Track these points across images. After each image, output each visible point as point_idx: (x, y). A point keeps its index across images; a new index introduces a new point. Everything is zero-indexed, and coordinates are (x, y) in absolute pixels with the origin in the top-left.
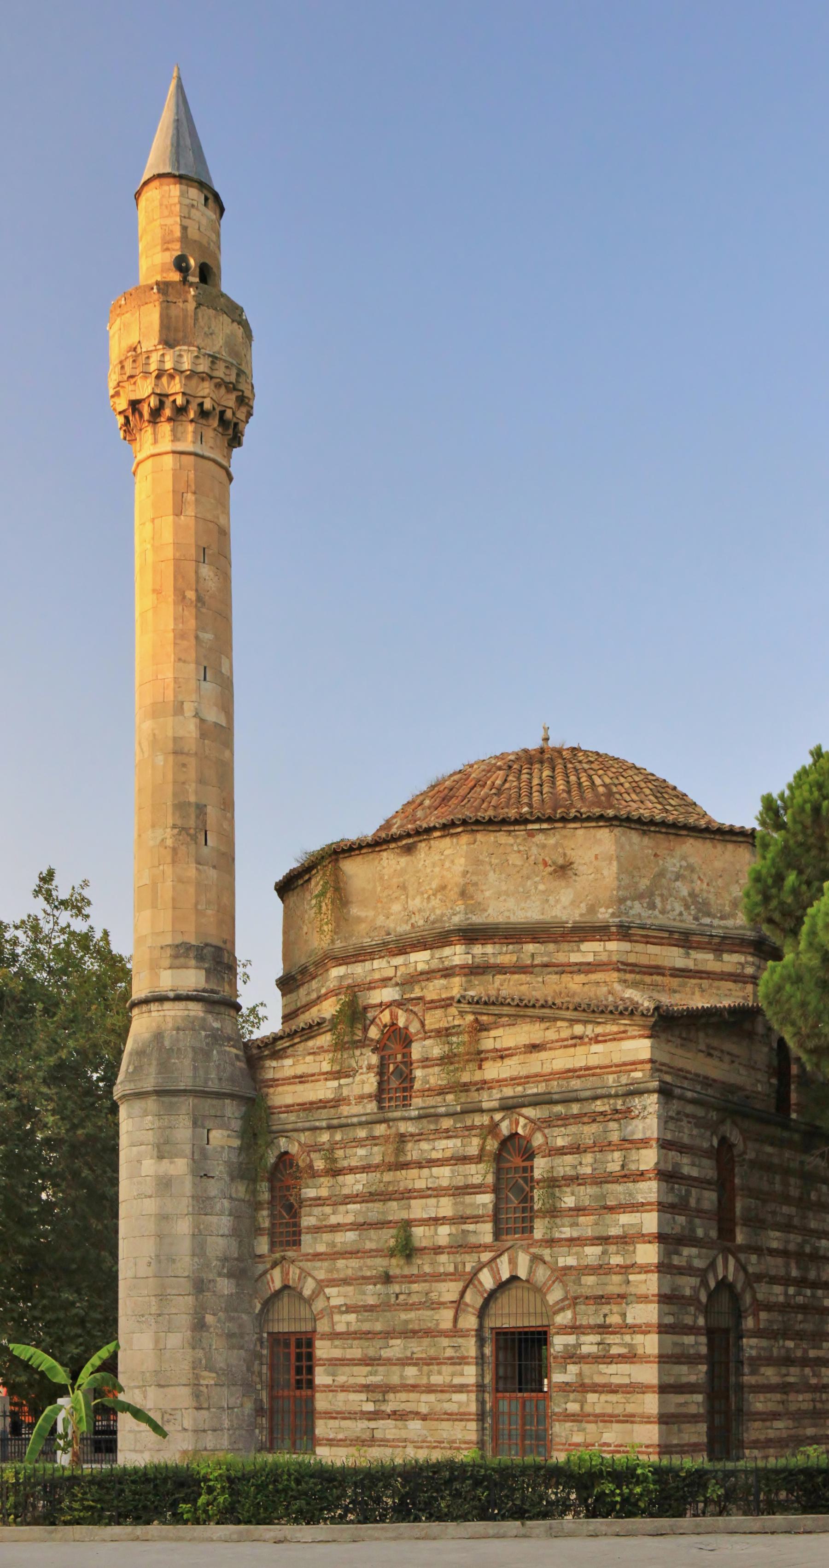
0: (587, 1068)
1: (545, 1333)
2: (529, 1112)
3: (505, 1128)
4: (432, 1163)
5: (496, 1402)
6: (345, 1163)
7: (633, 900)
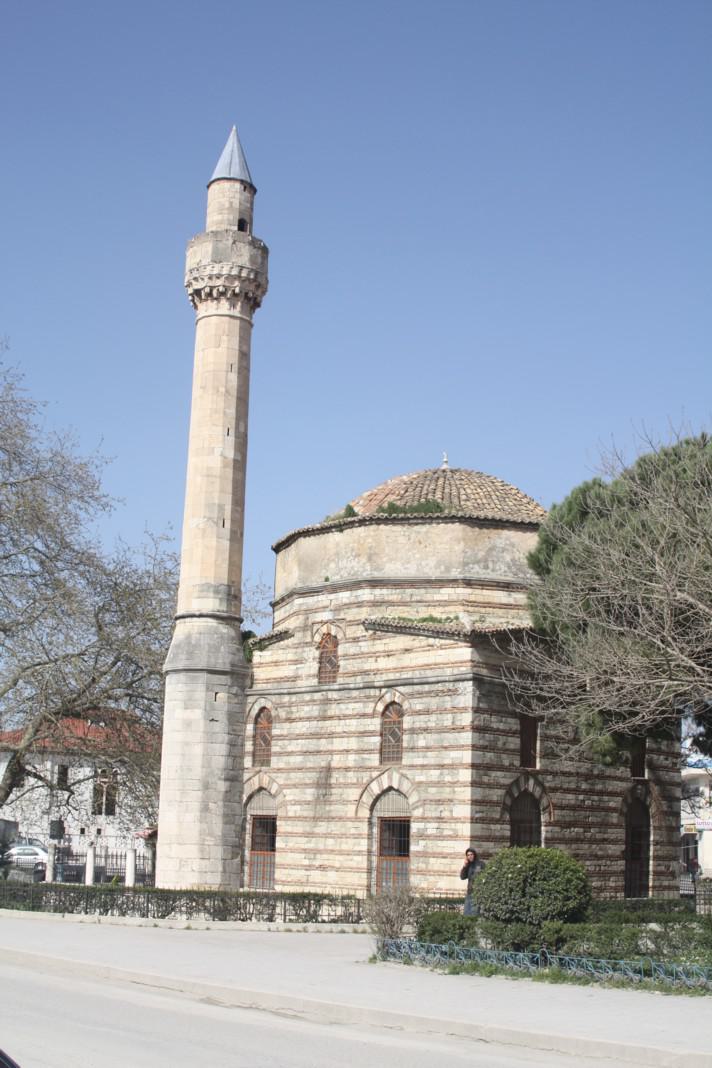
0: (436, 665)
1: (409, 821)
2: (401, 689)
3: (388, 698)
4: (346, 717)
5: (379, 862)
6: (297, 715)
7: (474, 564)
